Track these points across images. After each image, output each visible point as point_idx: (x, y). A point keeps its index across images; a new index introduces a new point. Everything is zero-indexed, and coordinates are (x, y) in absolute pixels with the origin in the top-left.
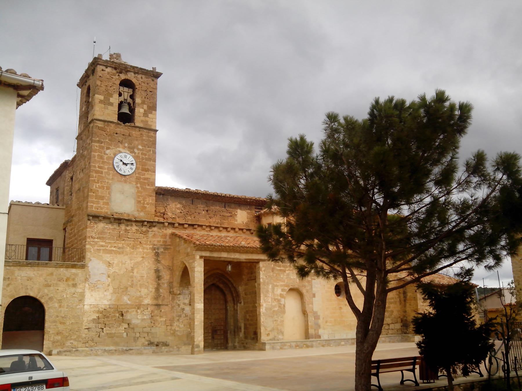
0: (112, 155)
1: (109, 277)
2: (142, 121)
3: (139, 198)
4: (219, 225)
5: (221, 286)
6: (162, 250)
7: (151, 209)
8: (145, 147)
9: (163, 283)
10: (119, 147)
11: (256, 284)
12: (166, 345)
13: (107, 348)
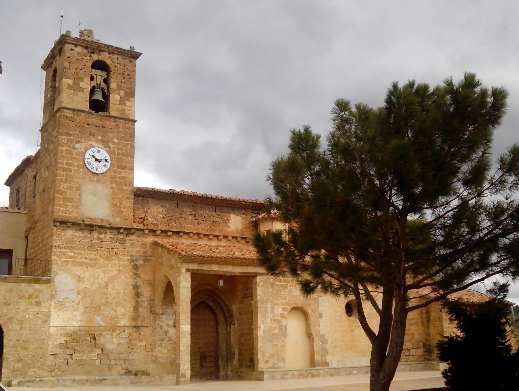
0: (83, 150)
1: (79, 293)
2: (118, 110)
3: (114, 201)
4: (208, 233)
5: (211, 304)
6: (142, 262)
7: (129, 213)
8: (121, 140)
9: (143, 301)
10: (90, 140)
11: (253, 302)
12: (146, 373)
13: (76, 378)
